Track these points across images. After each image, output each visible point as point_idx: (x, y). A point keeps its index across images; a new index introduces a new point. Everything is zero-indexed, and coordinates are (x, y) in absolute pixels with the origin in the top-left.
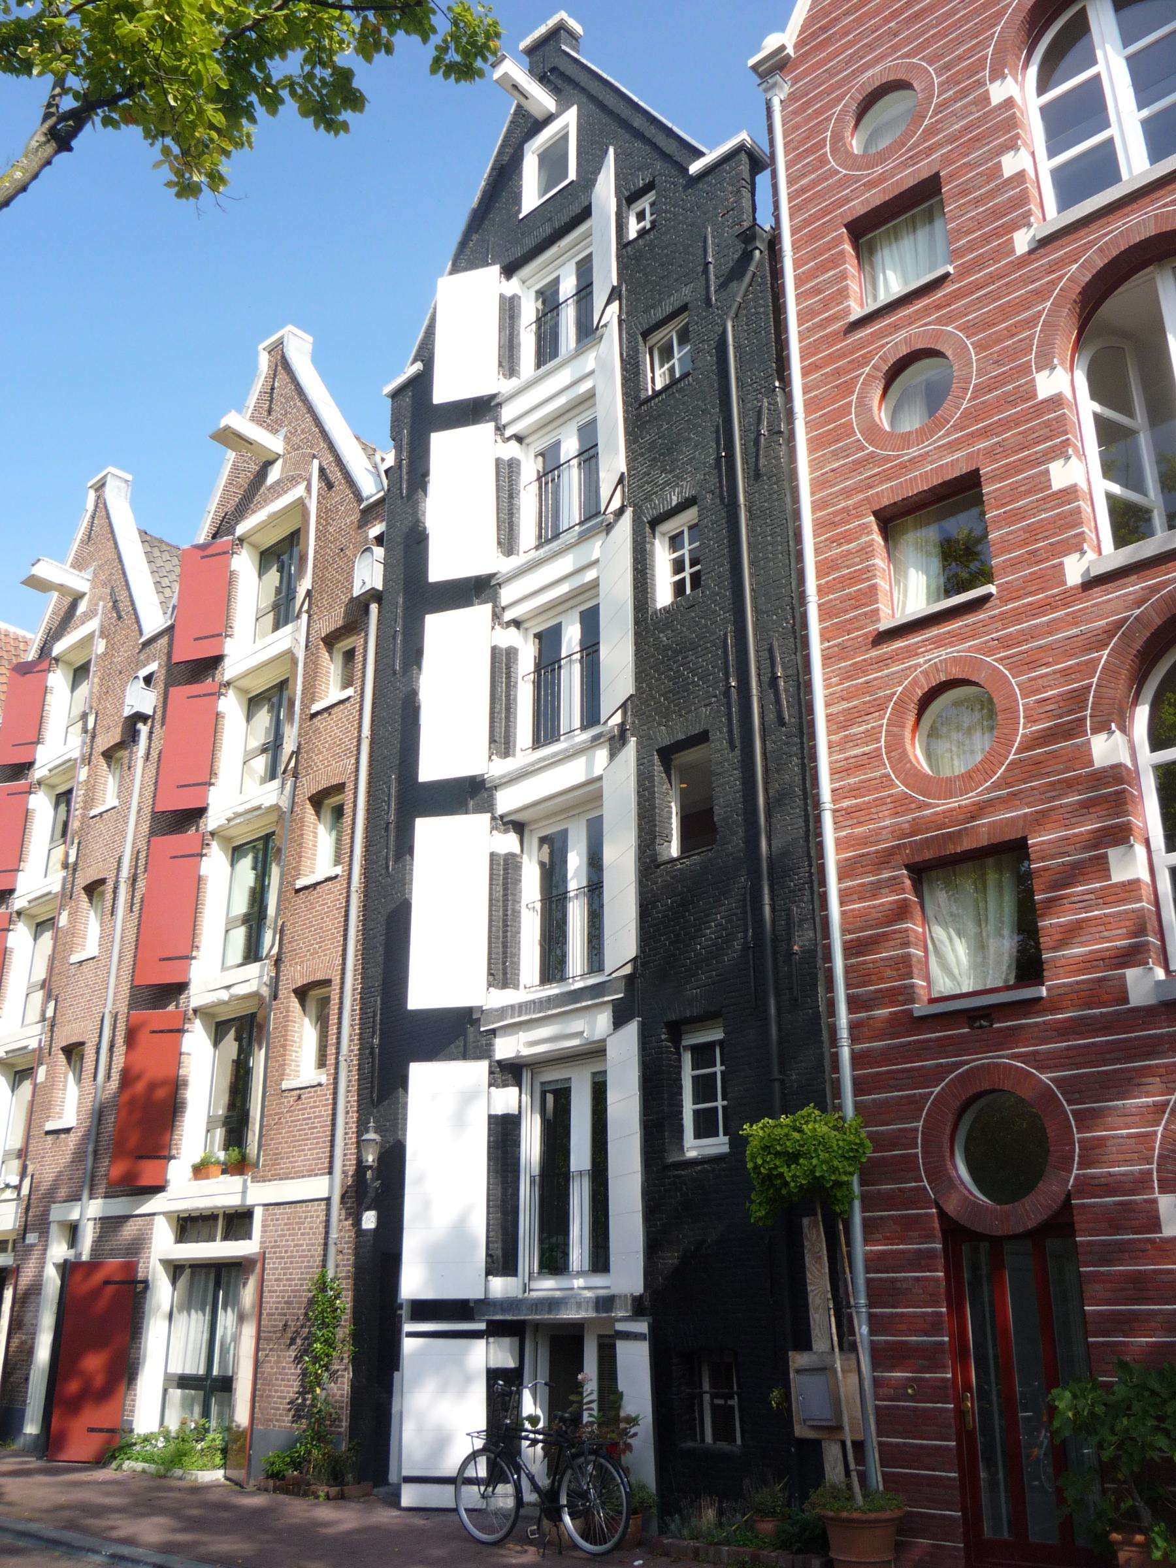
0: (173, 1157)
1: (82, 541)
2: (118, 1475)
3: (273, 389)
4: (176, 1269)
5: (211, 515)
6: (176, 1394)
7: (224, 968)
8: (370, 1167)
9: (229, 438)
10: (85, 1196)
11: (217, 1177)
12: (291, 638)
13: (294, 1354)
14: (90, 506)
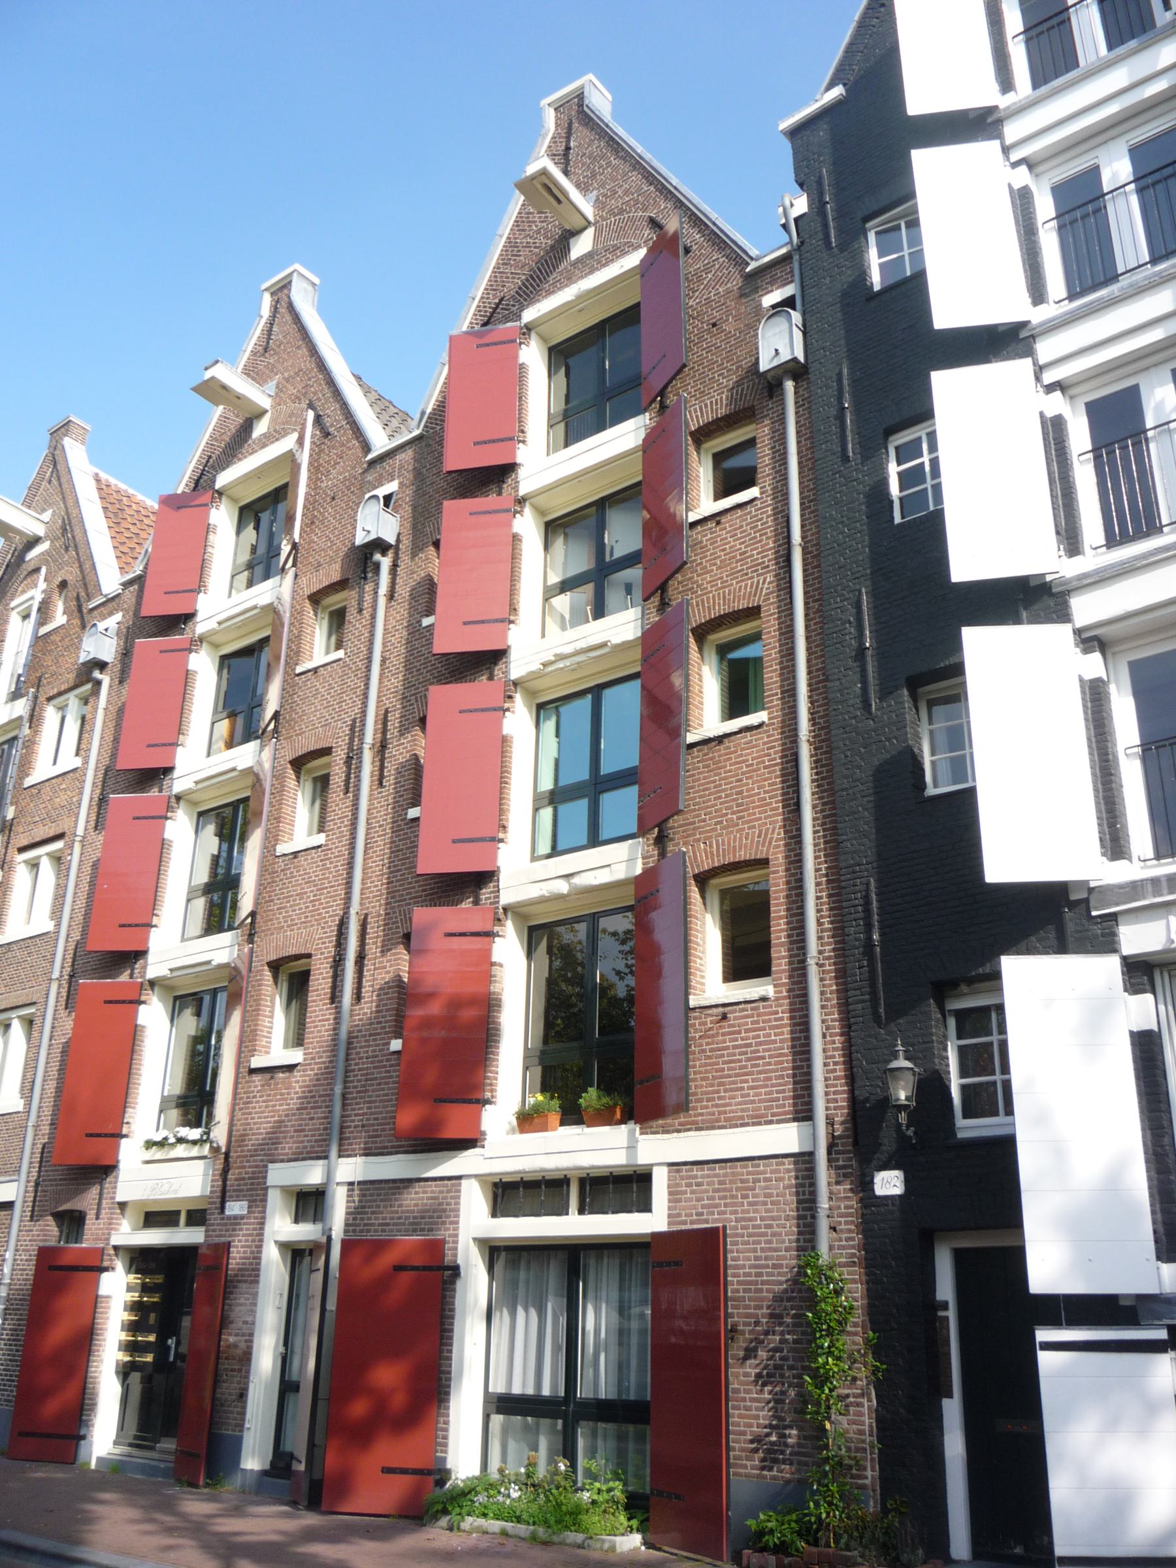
0: (488, 1102)
1: (254, 353)
2: (454, 1541)
3: (568, 148)
4: (494, 1251)
5: (476, 303)
6: (497, 1420)
7: (534, 858)
8: (905, 1107)
9: (213, 391)
10: (334, 1152)
11: (555, 1129)
12: (275, 591)
13: (754, 1372)
14: (266, 311)
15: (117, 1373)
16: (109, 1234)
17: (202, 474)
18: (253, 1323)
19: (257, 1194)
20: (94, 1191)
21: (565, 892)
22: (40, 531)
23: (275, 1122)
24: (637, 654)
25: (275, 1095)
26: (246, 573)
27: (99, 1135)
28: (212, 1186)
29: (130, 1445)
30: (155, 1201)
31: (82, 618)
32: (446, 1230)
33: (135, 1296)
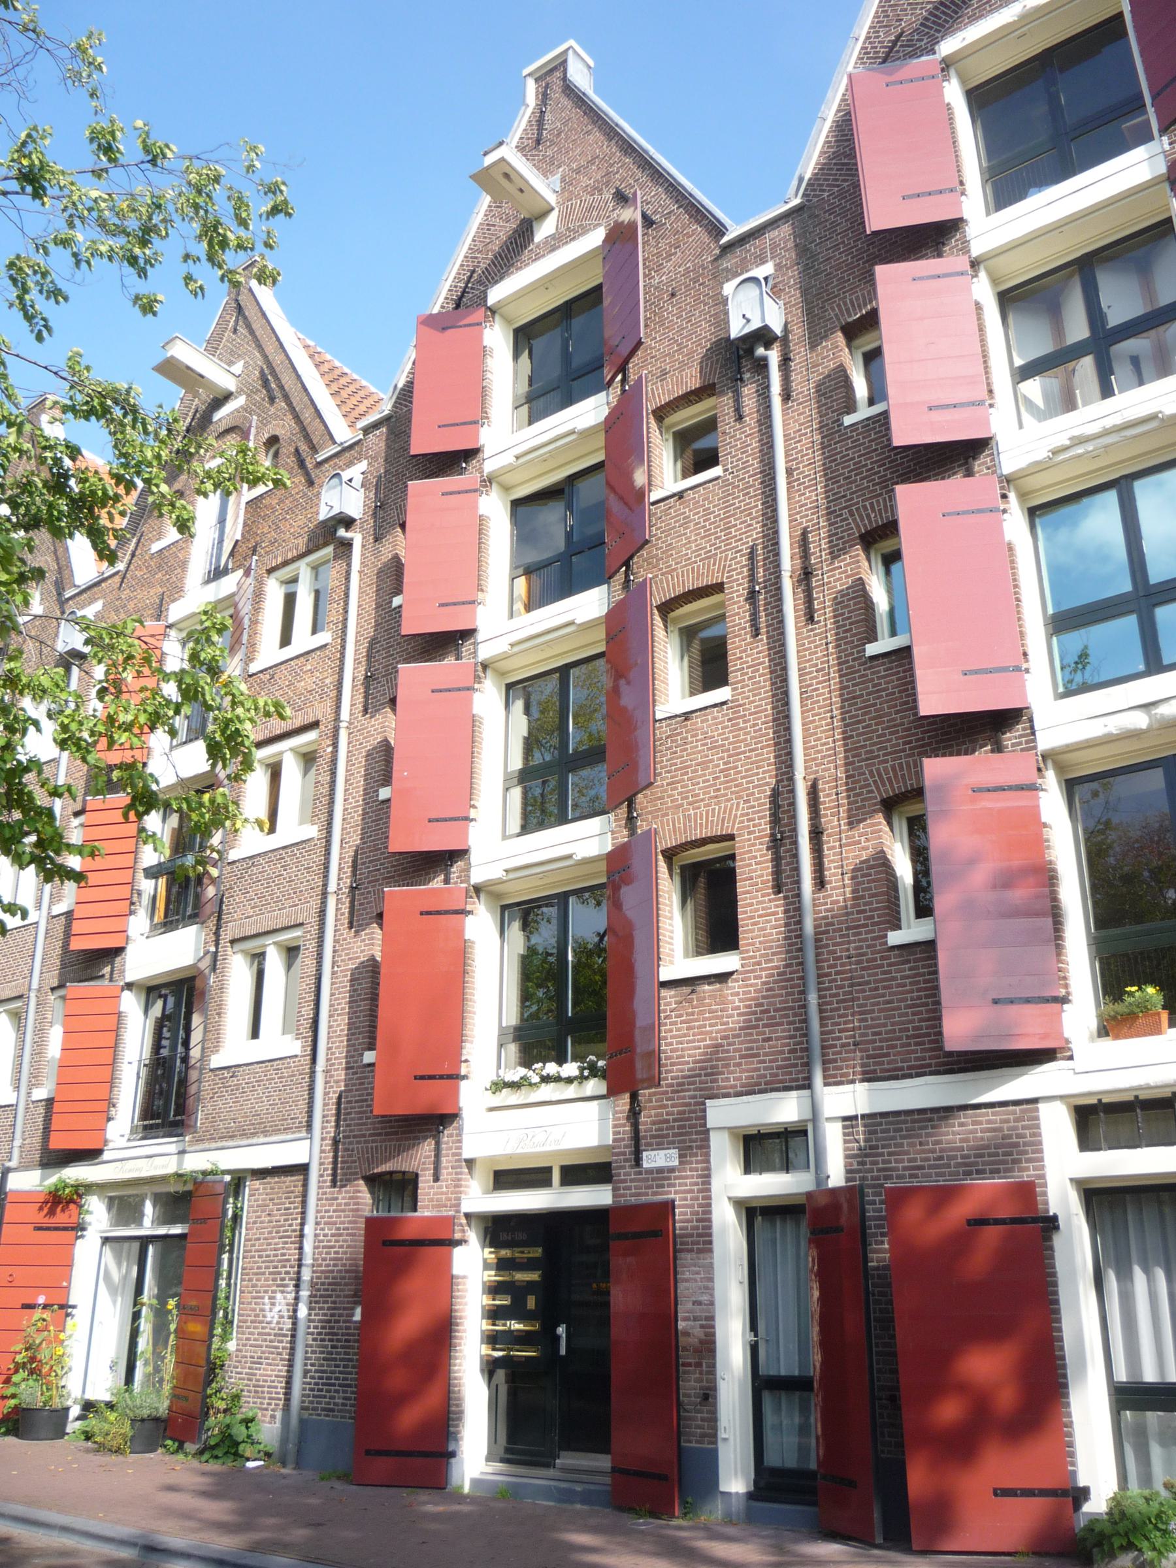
4: (1100, 1198)
7: (505, 837)
9: (496, 180)
10: (818, 1079)
15: (482, 1371)
16: (459, 1199)
17: (464, 292)
18: (712, 1303)
19: (692, 1137)
20: (427, 1148)
21: (1144, 726)
22: (230, 384)
23: (706, 1047)
24: (601, 634)
25: (701, 1013)
26: (526, 406)
27: (431, 1077)
28: (615, 1133)
29: (502, 1461)
30: (510, 1157)
31: (307, 474)
32: (1021, 1170)
33: (491, 1276)
